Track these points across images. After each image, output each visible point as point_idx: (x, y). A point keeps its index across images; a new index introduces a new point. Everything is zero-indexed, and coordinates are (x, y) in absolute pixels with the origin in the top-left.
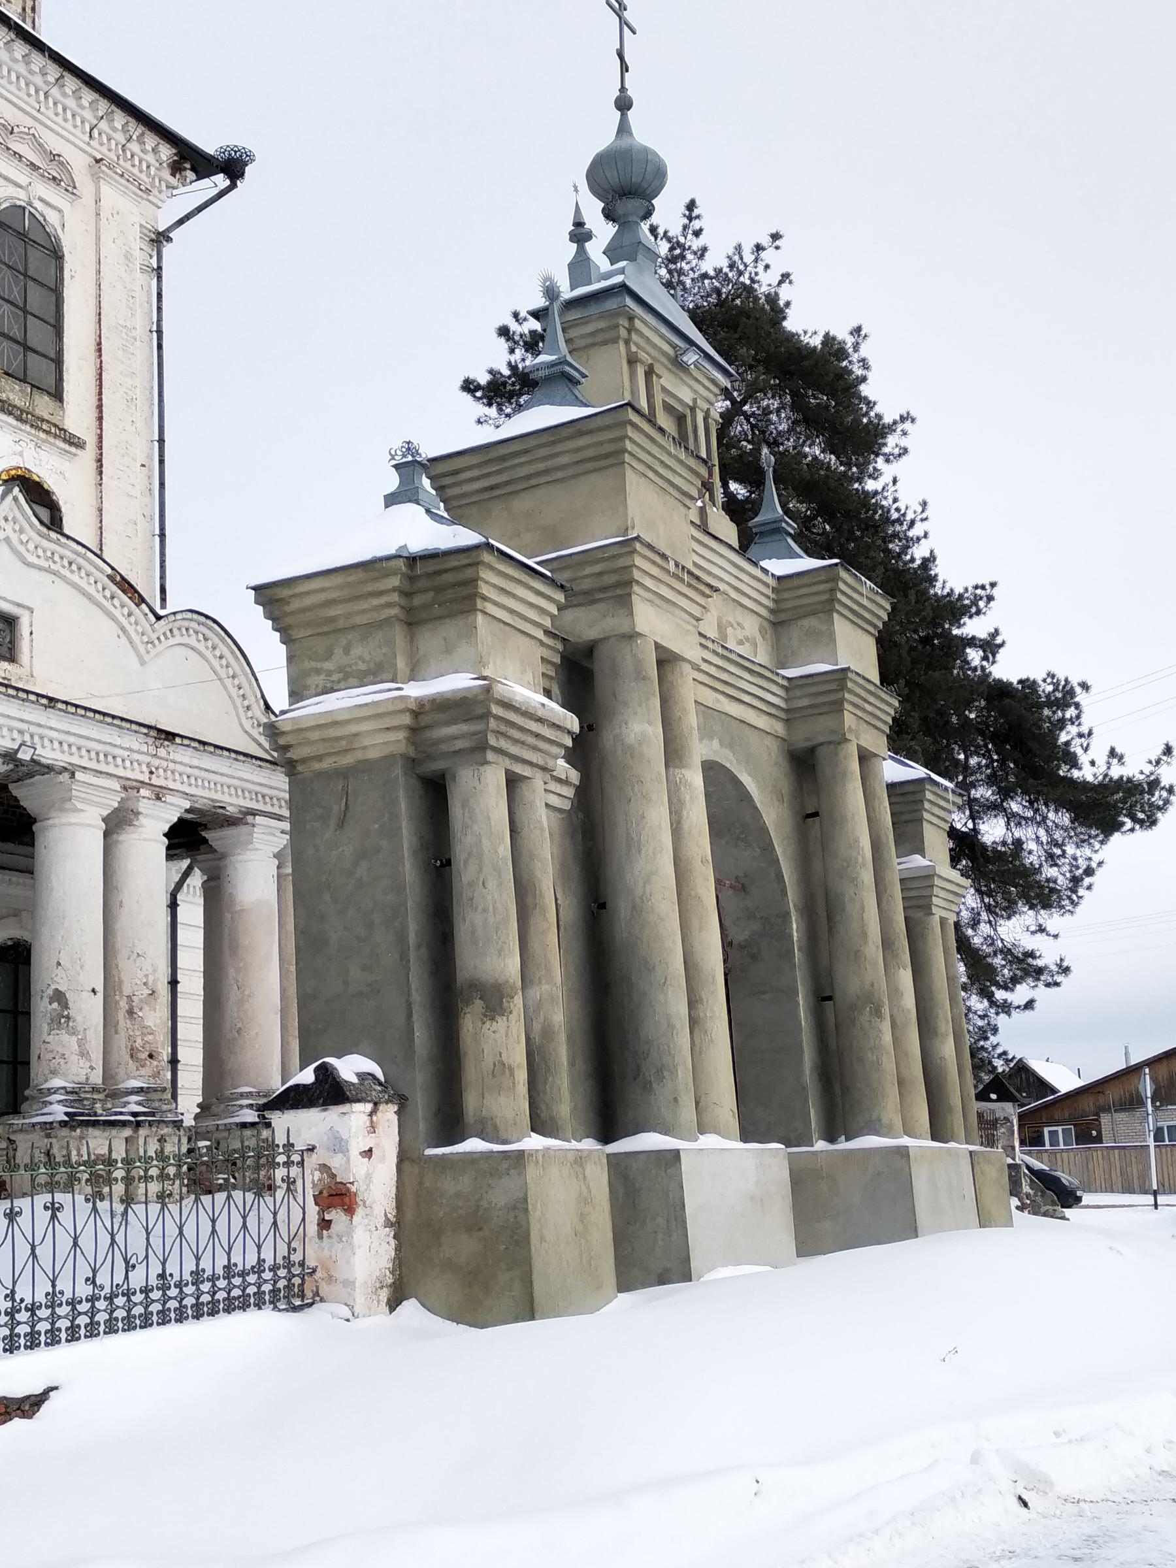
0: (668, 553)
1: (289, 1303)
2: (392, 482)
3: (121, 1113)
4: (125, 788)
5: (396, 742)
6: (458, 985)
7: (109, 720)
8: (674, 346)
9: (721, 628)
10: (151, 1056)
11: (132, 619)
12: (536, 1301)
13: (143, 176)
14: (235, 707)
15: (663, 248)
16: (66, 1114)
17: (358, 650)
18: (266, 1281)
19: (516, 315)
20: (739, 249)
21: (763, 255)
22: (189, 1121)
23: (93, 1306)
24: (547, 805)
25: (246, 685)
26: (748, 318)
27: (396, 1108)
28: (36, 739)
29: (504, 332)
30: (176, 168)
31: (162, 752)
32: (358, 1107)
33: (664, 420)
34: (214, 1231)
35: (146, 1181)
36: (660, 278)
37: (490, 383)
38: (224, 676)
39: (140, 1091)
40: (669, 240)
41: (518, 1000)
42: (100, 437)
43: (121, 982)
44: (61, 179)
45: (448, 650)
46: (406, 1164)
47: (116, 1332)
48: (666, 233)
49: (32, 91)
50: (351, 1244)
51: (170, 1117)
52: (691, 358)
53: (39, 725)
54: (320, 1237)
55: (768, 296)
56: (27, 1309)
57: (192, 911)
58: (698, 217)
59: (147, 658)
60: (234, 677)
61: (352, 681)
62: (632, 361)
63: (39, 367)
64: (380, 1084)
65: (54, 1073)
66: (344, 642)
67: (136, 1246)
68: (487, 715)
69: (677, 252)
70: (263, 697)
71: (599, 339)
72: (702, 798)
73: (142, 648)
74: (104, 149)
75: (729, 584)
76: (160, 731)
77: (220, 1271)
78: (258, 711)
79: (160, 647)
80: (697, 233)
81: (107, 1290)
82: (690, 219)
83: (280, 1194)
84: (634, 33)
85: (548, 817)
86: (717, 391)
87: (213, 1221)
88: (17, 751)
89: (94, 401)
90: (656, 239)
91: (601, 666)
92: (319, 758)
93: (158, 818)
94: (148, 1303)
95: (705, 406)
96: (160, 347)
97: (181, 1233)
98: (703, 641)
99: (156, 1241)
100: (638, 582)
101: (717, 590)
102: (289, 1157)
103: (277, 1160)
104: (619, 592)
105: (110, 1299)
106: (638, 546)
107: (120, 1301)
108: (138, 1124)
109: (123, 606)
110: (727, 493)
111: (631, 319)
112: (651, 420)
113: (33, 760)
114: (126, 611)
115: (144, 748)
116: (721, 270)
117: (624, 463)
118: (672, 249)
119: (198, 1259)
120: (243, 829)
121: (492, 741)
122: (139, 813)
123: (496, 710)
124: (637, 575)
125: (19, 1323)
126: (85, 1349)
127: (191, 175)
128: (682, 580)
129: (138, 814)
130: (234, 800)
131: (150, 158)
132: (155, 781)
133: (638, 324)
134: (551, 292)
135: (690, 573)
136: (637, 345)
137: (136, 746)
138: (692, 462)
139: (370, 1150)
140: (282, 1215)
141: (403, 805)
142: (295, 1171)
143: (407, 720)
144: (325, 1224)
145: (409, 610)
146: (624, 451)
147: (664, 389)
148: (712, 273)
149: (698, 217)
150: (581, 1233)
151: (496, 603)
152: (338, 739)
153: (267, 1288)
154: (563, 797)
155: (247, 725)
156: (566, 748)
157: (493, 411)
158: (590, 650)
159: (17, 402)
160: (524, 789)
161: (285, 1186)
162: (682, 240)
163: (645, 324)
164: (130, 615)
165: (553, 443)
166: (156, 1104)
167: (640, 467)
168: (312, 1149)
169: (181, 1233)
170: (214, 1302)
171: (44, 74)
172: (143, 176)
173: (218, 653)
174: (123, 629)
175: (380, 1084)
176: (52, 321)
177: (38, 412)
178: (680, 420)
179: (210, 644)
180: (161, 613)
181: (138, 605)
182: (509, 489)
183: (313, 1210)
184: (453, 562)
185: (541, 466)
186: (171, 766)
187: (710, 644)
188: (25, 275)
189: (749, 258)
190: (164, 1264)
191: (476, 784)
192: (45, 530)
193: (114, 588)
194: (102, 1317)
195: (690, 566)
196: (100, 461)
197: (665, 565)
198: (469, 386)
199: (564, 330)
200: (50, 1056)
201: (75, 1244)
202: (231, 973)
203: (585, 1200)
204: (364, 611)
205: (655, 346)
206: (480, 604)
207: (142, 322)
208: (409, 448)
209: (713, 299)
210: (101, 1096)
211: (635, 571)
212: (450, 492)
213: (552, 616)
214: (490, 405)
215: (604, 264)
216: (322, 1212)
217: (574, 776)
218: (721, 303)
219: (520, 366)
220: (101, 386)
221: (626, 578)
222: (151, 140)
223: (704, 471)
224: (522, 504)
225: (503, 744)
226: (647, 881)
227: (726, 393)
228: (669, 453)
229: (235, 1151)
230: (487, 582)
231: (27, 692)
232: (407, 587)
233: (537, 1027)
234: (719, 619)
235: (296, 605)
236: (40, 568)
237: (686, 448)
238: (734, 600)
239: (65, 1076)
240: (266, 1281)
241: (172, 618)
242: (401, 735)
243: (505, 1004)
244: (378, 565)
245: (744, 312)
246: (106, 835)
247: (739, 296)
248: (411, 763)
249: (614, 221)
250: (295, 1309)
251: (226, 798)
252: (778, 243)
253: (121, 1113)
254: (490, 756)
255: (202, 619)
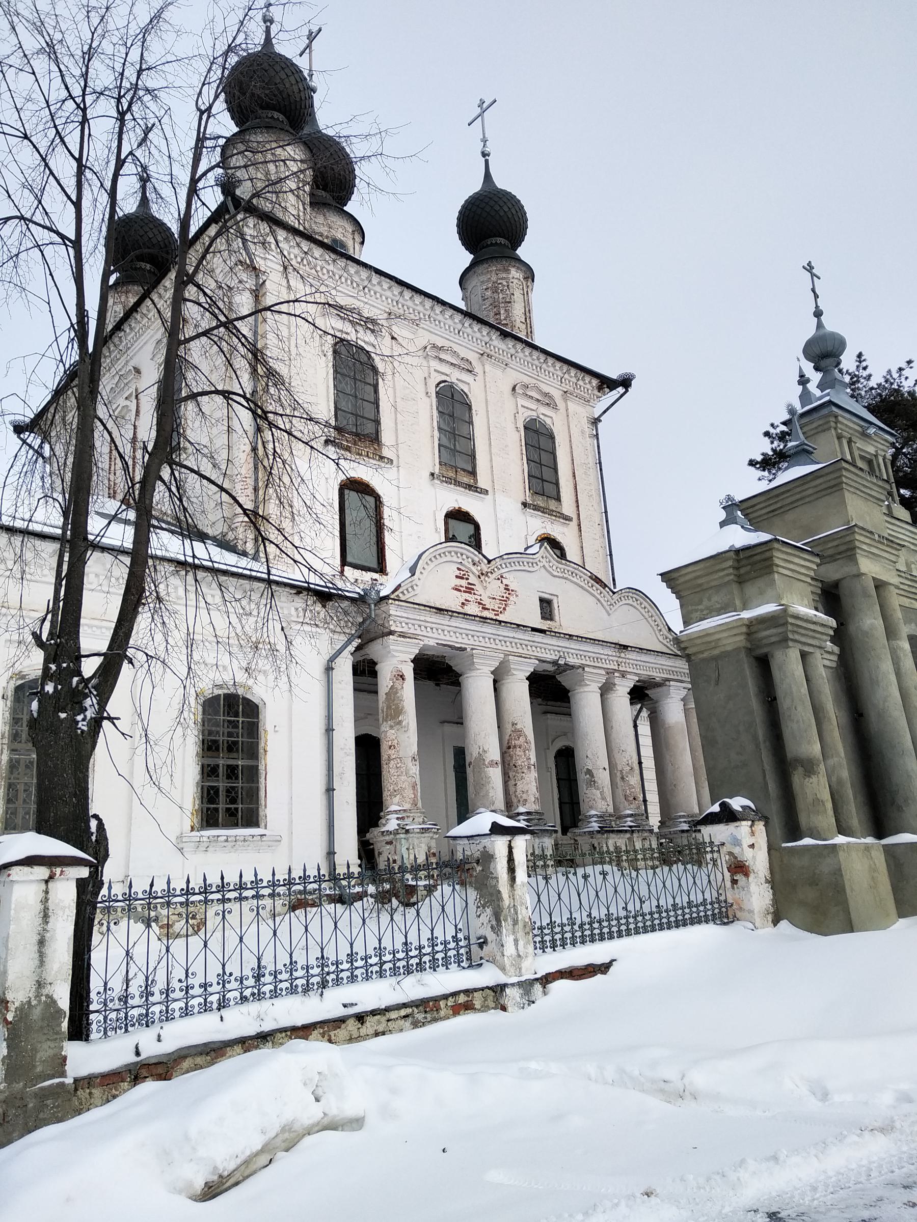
0: (873, 531)
1: (721, 921)
2: (723, 515)
3: (624, 826)
4: (608, 673)
5: (740, 641)
6: (789, 760)
7: (597, 642)
8: (861, 427)
9: (908, 565)
10: (634, 799)
11: (602, 595)
12: (853, 924)
13: (586, 395)
14: (654, 631)
15: (847, 379)
16: (599, 827)
17: (715, 598)
18: (708, 910)
19: (772, 425)
20: (889, 372)
21: (903, 372)
22: (656, 830)
23: (627, 921)
24: (824, 666)
25: (658, 620)
26: (900, 405)
27: (763, 823)
28: (566, 654)
29: (767, 434)
30: (600, 388)
31: (623, 655)
32: (744, 823)
33: (860, 464)
34: (680, 885)
35: (645, 861)
36: (847, 393)
37: (763, 460)
38: (647, 617)
39: (631, 815)
40: (850, 374)
41: (822, 766)
42: (579, 515)
43: (616, 764)
44: (550, 403)
45: (761, 593)
46: (772, 852)
47: (640, 933)
48: (847, 371)
49: (534, 367)
50: (749, 892)
51: (647, 828)
52: (872, 431)
53: (566, 648)
54: (733, 888)
55: (909, 393)
56: (597, 922)
57: (645, 729)
58: (864, 360)
59: (610, 612)
60: (652, 616)
61: (714, 613)
62: (839, 437)
63: (549, 488)
64: (754, 811)
65: (591, 808)
66: (708, 595)
67: (644, 892)
68: (786, 623)
69: (855, 379)
70: (667, 624)
71: (820, 429)
72: (910, 654)
73: (608, 608)
74: (568, 387)
75: (909, 542)
76: (621, 645)
77: (685, 904)
78: (665, 631)
79: (616, 607)
80: (865, 368)
81: (633, 913)
82: (860, 362)
83: (710, 866)
84: (819, 278)
85: (825, 671)
86: (888, 445)
87: (679, 880)
88: (558, 660)
89: (574, 499)
90: (842, 374)
91: (843, 591)
92: (702, 652)
93: (624, 686)
94: (653, 920)
95: (883, 453)
96: (601, 470)
97: (664, 885)
98: (899, 573)
99: (653, 889)
100: (859, 548)
101: (904, 546)
102: (712, 848)
103: (707, 850)
104: (849, 553)
105: (635, 917)
106: (856, 530)
107: (640, 919)
108: (633, 831)
109: (597, 590)
110: (900, 495)
111: (836, 417)
112: (855, 466)
113: (565, 664)
114: (599, 592)
115: (614, 654)
116: (880, 384)
117: (843, 489)
118: (851, 379)
119: (674, 898)
120: (664, 688)
121: (790, 636)
122: (615, 684)
123: (790, 620)
124: (857, 544)
125: (595, 929)
126: (626, 941)
127: (607, 390)
128: (883, 544)
129: (615, 684)
130: (659, 675)
131: (588, 386)
132: (621, 669)
133: (840, 418)
134: (792, 411)
135: (887, 539)
136: (841, 429)
137: (610, 653)
138: (880, 483)
139: (753, 844)
140: (712, 877)
141: (748, 672)
142: (716, 855)
143: (744, 629)
144: (734, 882)
145: (739, 576)
146: (842, 482)
147: (859, 448)
148: (876, 386)
149: (864, 360)
150: (874, 885)
151: (784, 567)
152: (710, 642)
153: (709, 913)
154: (831, 661)
155: (661, 638)
156: (831, 636)
157: (766, 473)
158: (836, 584)
159: (541, 505)
160: (810, 659)
161: (712, 863)
162: (857, 373)
163: (844, 418)
164: (601, 593)
165: (803, 484)
166: (640, 822)
167: (852, 490)
168: (723, 844)
169: (664, 885)
170: (684, 920)
171: (538, 359)
172: (586, 395)
173: (643, 606)
174: (598, 600)
175: (754, 811)
176: (553, 467)
177: (551, 508)
178: (870, 462)
179: (639, 602)
180: (615, 590)
181: (604, 588)
182: (782, 510)
183: (727, 875)
184: (759, 550)
185: (798, 496)
186: (628, 661)
187: (903, 575)
188: (539, 448)
189: (895, 375)
190: (658, 901)
191: (785, 658)
192: (559, 560)
193: (593, 582)
194: (632, 926)
195: (886, 535)
196: (579, 525)
197: (873, 537)
198: (752, 463)
199: (801, 428)
200: (588, 800)
201: (616, 891)
202: (668, 757)
203: (873, 870)
204: (715, 579)
205: (850, 428)
206: (775, 569)
207: (591, 460)
208: (729, 498)
209: (878, 399)
210: (614, 818)
211: (856, 542)
212: (751, 516)
213: (814, 570)
214: (764, 470)
215: (818, 393)
216: (732, 876)
217: (836, 650)
218: (882, 401)
219: (778, 449)
220: (577, 492)
221: (852, 546)
222: (588, 378)
223: (887, 486)
224: (790, 516)
225: (797, 637)
226: (885, 701)
227: (893, 445)
228: (867, 480)
229: (685, 846)
230: (778, 558)
231: (560, 633)
232: (736, 565)
233: (834, 779)
234: (906, 561)
235: (682, 580)
236: (559, 577)
237: (876, 476)
238: (913, 550)
239: (596, 810)
240: (708, 910)
241: (620, 592)
242: (742, 637)
243: (815, 769)
244: (721, 556)
245: (896, 403)
246: (601, 695)
247: (893, 395)
248: (749, 650)
249: (820, 371)
250: (725, 924)
251: (655, 674)
252: (911, 365)
253: (624, 826)
254: (790, 643)
255: (634, 591)
